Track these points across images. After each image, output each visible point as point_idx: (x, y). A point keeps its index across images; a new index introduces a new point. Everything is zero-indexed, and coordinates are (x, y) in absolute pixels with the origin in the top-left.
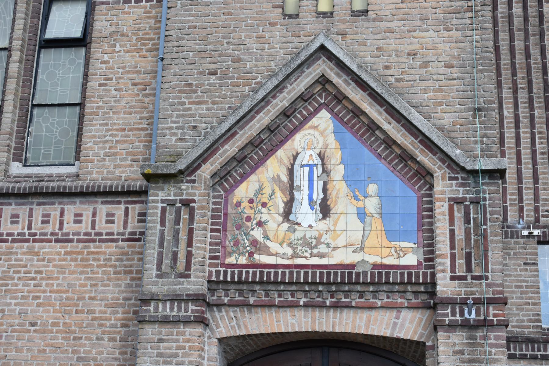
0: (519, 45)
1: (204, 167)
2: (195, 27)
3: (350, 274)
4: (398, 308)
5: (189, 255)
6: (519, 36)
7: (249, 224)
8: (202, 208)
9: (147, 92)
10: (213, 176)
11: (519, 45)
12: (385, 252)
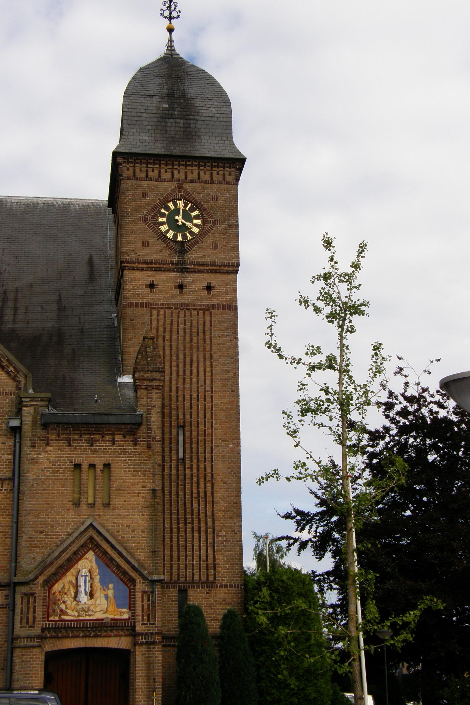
0: (174, 490)
1: (40, 578)
2: (32, 510)
3: (102, 623)
4: (120, 636)
5: (34, 617)
6: (174, 485)
7: (59, 602)
8: (40, 596)
9: (7, 536)
10: (44, 582)
11: (174, 490)
12: (116, 613)
